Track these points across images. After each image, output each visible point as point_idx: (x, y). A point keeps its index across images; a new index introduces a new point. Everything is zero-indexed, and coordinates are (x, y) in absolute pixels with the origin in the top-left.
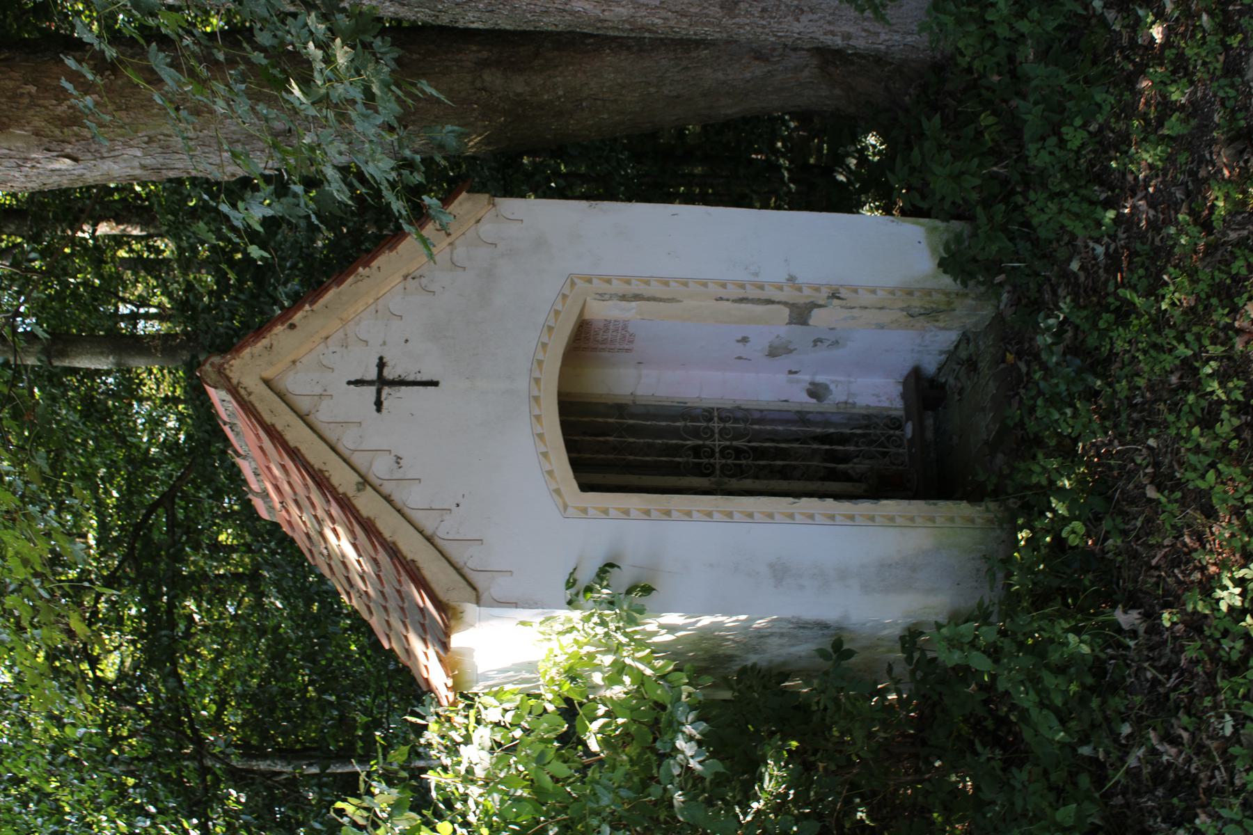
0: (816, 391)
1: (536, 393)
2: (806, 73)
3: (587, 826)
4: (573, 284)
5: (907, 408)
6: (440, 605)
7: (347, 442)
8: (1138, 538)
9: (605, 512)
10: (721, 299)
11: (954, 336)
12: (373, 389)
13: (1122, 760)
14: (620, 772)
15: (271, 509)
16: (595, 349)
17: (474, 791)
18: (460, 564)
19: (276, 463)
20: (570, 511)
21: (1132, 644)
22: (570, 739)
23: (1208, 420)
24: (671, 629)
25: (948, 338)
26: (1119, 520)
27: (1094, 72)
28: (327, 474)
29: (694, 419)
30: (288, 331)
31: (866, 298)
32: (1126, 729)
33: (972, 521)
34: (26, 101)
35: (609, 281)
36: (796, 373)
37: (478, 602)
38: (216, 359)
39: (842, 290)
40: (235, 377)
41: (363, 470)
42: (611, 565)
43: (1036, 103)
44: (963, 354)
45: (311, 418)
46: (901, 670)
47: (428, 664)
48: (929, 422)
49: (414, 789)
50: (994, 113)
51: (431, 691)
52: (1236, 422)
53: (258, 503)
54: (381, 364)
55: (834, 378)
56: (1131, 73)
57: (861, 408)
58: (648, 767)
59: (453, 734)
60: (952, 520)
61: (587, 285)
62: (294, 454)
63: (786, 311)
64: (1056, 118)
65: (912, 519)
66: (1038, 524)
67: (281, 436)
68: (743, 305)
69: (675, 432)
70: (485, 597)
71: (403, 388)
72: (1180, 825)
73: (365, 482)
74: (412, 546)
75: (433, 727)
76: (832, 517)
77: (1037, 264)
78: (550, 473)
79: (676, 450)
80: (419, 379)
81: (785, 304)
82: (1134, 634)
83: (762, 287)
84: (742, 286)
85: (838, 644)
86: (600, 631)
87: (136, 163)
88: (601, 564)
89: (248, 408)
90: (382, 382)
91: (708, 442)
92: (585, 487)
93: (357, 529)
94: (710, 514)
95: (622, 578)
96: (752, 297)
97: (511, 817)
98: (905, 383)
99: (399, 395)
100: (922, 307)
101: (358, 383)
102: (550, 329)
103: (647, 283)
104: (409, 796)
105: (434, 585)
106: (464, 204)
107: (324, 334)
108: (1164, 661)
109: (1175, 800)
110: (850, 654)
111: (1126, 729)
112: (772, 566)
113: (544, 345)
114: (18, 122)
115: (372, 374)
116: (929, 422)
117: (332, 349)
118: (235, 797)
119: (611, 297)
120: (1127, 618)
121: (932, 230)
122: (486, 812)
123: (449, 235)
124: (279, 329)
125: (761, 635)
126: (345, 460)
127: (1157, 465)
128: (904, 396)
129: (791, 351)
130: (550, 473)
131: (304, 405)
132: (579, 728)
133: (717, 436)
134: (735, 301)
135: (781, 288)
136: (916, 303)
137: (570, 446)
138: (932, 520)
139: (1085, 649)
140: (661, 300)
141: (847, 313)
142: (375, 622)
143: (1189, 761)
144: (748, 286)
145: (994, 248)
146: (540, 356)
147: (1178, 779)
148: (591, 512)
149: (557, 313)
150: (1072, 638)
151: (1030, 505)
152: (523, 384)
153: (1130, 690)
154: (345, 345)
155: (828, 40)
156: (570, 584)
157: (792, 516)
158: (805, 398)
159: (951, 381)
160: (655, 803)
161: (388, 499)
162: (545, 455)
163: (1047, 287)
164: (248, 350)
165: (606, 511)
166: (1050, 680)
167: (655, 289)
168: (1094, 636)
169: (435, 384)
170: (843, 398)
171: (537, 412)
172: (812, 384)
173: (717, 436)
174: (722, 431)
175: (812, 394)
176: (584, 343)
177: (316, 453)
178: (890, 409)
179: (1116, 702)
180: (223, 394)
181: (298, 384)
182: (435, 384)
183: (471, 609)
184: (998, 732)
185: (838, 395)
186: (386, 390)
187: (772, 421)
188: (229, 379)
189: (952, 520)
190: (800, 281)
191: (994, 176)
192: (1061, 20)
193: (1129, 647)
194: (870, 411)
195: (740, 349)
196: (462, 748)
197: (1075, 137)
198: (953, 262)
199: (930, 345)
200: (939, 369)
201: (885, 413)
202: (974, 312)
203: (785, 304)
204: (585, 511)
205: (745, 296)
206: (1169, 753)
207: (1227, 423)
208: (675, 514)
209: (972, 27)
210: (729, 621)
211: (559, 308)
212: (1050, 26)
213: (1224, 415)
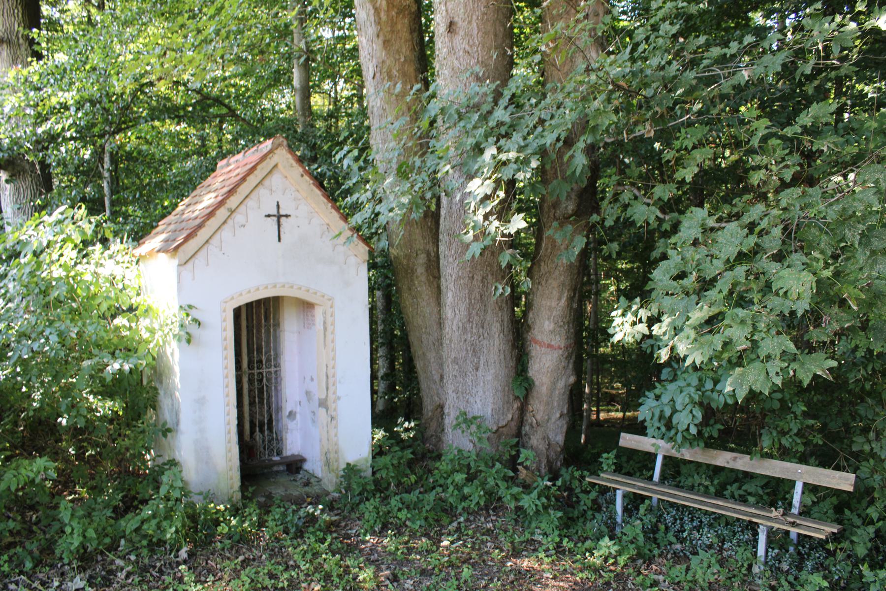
0: (292, 415)
2: (437, 399)
3: (78, 320)
4: (329, 300)
5: (287, 457)
6: (177, 248)
7: (250, 203)
8: (221, 555)
9: (224, 321)
11: (320, 476)
12: (275, 213)
13: (119, 557)
14: (104, 335)
15: (222, 167)
17: (92, 268)
18: (196, 256)
19: (242, 171)
21: (172, 556)
22: (117, 312)
23: (272, 576)
24: (172, 354)
25: (319, 473)
26: (229, 546)
27: (431, 520)
29: (275, 359)
31: (332, 432)
32: (133, 558)
33: (231, 488)
34: (397, 57)
35: (332, 316)
37: (179, 265)
38: (285, 143)
40: (278, 151)
41: (238, 210)
42: (199, 324)
43: (418, 498)
44: (312, 480)
45: (260, 186)
46: (160, 461)
47: (153, 242)
48: (281, 468)
49: (92, 240)
50: (416, 482)
51: (139, 245)
52: (269, 587)
53: (225, 161)
54: (287, 216)
56: (429, 534)
58: (107, 347)
59: (120, 255)
60: (231, 479)
62: (244, 179)
63: (324, 397)
64: (412, 507)
65: (230, 460)
66: (227, 513)
69: (268, 352)
70: (182, 268)
72: (88, 581)
73: (232, 211)
74: (203, 234)
75: (122, 247)
76: (229, 424)
77: (348, 506)
79: (259, 350)
82: (177, 556)
83: (334, 385)
84: (333, 376)
85: (170, 430)
86: (169, 322)
87: (374, 103)
88: (200, 319)
89: (263, 158)
92: (237, 312)
93: (211, 209)
96: (329, 380)
97: (80, 285)
98: (298, 455)
101: (278, 206)
102: (308, 291)
103: (332, 333)
104: (89, 238)
108: (164, 570)
109: (99, 579)
110: (165, 436)
111: (133, 558)
113: (300, 288)
114: (388, 53)
115: (282, 212)
116: (281, 468)
118: (87, 154)
119: (325, 317)
120: (183, 554)
122: (82, 274)
124: (301, 170)
125: (172, 396)
126: (242, 202)
127: (254, 560)
128: (293, 455)
129: (309, 401)
131: (267, 182)
132: (124, 314)
135: (334, 393)
136: (332, 456)
137: (258, 302)
138: (231, 470)
139: (168, 536)
142: (170, 218)
143: (118, 582)
145: (355, 487)
146: (295, 287)
147: (110, 580)
149: (316, 293)
150: (174, 529)
151: (235, 511)
153: (151, 557)
154: (295, 199)
155: (446, 406)
156: (190, 307)
158: (288, 410)
159: (300, 476)
160: (90, 352)
161: (225, 222)
163: (339, 511)
166: (154, 522)
167: (329, 337)
168: (175, 539)
169: (279, 240)
170: (289, 427)
174: (270, 373)
175: (291, 413)
176: (306, 306)
177: (244, 189)
179: (145, 552)
180: (269, 147)
181: (276, 180)
182: (279, 240)
183: (175, 262)
184: (130, 504)
185: (291, 425)
186: (275, 219)
187: (277, 396)
189: (231, 479)
190: (339, 402)
191: (389, 484)
192: (454, 505)
193: (170, 554)
196: (112, 261)
197: (402, 515)
198: (351, 470)
199: (314, 465)
202: (330, 482)
204: (224, 311)
206: (121, 575)
207: (268, 583)
208: (225, 352)
209: (450, 467)
210: (177, 380)
212: (451, 500)
213: (273, 581)
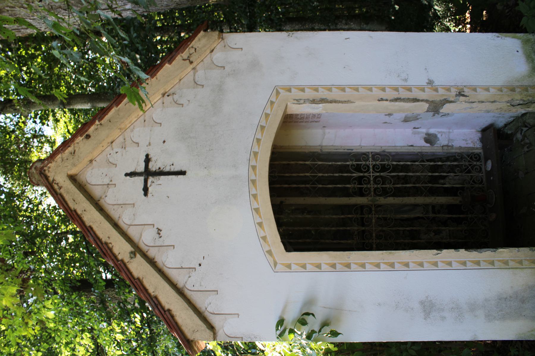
0: (430, 139)
1: (253, 177)
4: (278, 93)
5: (484, 147)
10: (382, 100)
12: (142, 178)
16: (297, 122)
20: (279, 266)
28: (110, 246)
30: (85, 140)
35: (303, 90)
36: (418, 128)
39: (466, 90)
40: (51, 175)
45: (102, 202)
54: (148, 160)
55: (440, 130)
57: (456, 148)
61: (288, 93)
65: (521, 262)
67: (80, 218)
68: (397, 103)
71: (162, 177)
73: (137, 250)
78: (264, 238)
79: (348, 180)
80: (172, 170)
81: (427, 101)
83: (410, 90)
84: (396, 90)
90: (148, 173)
91: (366, 174)
92: (288, 249)
94: (378, 265)
95: (314, 324)
99: (159, 182)
100: (521, 100)
102: (263, 128)
103: (330, 90)
105: (184, 328)
106: (202, 41)
107: (110, 140)
112: (422, 303)
113: (258, 140)
117: (116, 150)
121: (526, 42)
123: (191, 63)
128: (482, 140)
130: (264, 238)
131: (97, 192)
133: (371, 170)
134: (392, 101)
140: (339, 102)
141: (468, 105)
144: (400, 90)
146: (256, 149)
148: (294, 267)
149: (267, 115)
152: (243, 170)
156: (281, 322)
157: (436, 264)
158: (423, 143)
162: (260, 224)
164: (60, 156)
165: (304, 266)
167: (336, 94)
170: (445, 143)
171: (254, 192)
172: (428, 134)
173: (371, 170)
175: (427, 141)
176: (289, 121)
178: (473, 148)
181: (93, 178)
185: (443, 141)
186: (151, 179)
188: (47, 178)
194: (462, 151)
195: (387, 119)
200: (506, 125)
201: (471, 151)
203: (427, 101)
205: (399, 96)
211: (268, 111)
